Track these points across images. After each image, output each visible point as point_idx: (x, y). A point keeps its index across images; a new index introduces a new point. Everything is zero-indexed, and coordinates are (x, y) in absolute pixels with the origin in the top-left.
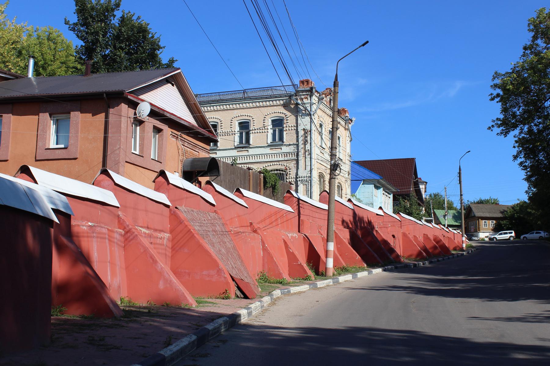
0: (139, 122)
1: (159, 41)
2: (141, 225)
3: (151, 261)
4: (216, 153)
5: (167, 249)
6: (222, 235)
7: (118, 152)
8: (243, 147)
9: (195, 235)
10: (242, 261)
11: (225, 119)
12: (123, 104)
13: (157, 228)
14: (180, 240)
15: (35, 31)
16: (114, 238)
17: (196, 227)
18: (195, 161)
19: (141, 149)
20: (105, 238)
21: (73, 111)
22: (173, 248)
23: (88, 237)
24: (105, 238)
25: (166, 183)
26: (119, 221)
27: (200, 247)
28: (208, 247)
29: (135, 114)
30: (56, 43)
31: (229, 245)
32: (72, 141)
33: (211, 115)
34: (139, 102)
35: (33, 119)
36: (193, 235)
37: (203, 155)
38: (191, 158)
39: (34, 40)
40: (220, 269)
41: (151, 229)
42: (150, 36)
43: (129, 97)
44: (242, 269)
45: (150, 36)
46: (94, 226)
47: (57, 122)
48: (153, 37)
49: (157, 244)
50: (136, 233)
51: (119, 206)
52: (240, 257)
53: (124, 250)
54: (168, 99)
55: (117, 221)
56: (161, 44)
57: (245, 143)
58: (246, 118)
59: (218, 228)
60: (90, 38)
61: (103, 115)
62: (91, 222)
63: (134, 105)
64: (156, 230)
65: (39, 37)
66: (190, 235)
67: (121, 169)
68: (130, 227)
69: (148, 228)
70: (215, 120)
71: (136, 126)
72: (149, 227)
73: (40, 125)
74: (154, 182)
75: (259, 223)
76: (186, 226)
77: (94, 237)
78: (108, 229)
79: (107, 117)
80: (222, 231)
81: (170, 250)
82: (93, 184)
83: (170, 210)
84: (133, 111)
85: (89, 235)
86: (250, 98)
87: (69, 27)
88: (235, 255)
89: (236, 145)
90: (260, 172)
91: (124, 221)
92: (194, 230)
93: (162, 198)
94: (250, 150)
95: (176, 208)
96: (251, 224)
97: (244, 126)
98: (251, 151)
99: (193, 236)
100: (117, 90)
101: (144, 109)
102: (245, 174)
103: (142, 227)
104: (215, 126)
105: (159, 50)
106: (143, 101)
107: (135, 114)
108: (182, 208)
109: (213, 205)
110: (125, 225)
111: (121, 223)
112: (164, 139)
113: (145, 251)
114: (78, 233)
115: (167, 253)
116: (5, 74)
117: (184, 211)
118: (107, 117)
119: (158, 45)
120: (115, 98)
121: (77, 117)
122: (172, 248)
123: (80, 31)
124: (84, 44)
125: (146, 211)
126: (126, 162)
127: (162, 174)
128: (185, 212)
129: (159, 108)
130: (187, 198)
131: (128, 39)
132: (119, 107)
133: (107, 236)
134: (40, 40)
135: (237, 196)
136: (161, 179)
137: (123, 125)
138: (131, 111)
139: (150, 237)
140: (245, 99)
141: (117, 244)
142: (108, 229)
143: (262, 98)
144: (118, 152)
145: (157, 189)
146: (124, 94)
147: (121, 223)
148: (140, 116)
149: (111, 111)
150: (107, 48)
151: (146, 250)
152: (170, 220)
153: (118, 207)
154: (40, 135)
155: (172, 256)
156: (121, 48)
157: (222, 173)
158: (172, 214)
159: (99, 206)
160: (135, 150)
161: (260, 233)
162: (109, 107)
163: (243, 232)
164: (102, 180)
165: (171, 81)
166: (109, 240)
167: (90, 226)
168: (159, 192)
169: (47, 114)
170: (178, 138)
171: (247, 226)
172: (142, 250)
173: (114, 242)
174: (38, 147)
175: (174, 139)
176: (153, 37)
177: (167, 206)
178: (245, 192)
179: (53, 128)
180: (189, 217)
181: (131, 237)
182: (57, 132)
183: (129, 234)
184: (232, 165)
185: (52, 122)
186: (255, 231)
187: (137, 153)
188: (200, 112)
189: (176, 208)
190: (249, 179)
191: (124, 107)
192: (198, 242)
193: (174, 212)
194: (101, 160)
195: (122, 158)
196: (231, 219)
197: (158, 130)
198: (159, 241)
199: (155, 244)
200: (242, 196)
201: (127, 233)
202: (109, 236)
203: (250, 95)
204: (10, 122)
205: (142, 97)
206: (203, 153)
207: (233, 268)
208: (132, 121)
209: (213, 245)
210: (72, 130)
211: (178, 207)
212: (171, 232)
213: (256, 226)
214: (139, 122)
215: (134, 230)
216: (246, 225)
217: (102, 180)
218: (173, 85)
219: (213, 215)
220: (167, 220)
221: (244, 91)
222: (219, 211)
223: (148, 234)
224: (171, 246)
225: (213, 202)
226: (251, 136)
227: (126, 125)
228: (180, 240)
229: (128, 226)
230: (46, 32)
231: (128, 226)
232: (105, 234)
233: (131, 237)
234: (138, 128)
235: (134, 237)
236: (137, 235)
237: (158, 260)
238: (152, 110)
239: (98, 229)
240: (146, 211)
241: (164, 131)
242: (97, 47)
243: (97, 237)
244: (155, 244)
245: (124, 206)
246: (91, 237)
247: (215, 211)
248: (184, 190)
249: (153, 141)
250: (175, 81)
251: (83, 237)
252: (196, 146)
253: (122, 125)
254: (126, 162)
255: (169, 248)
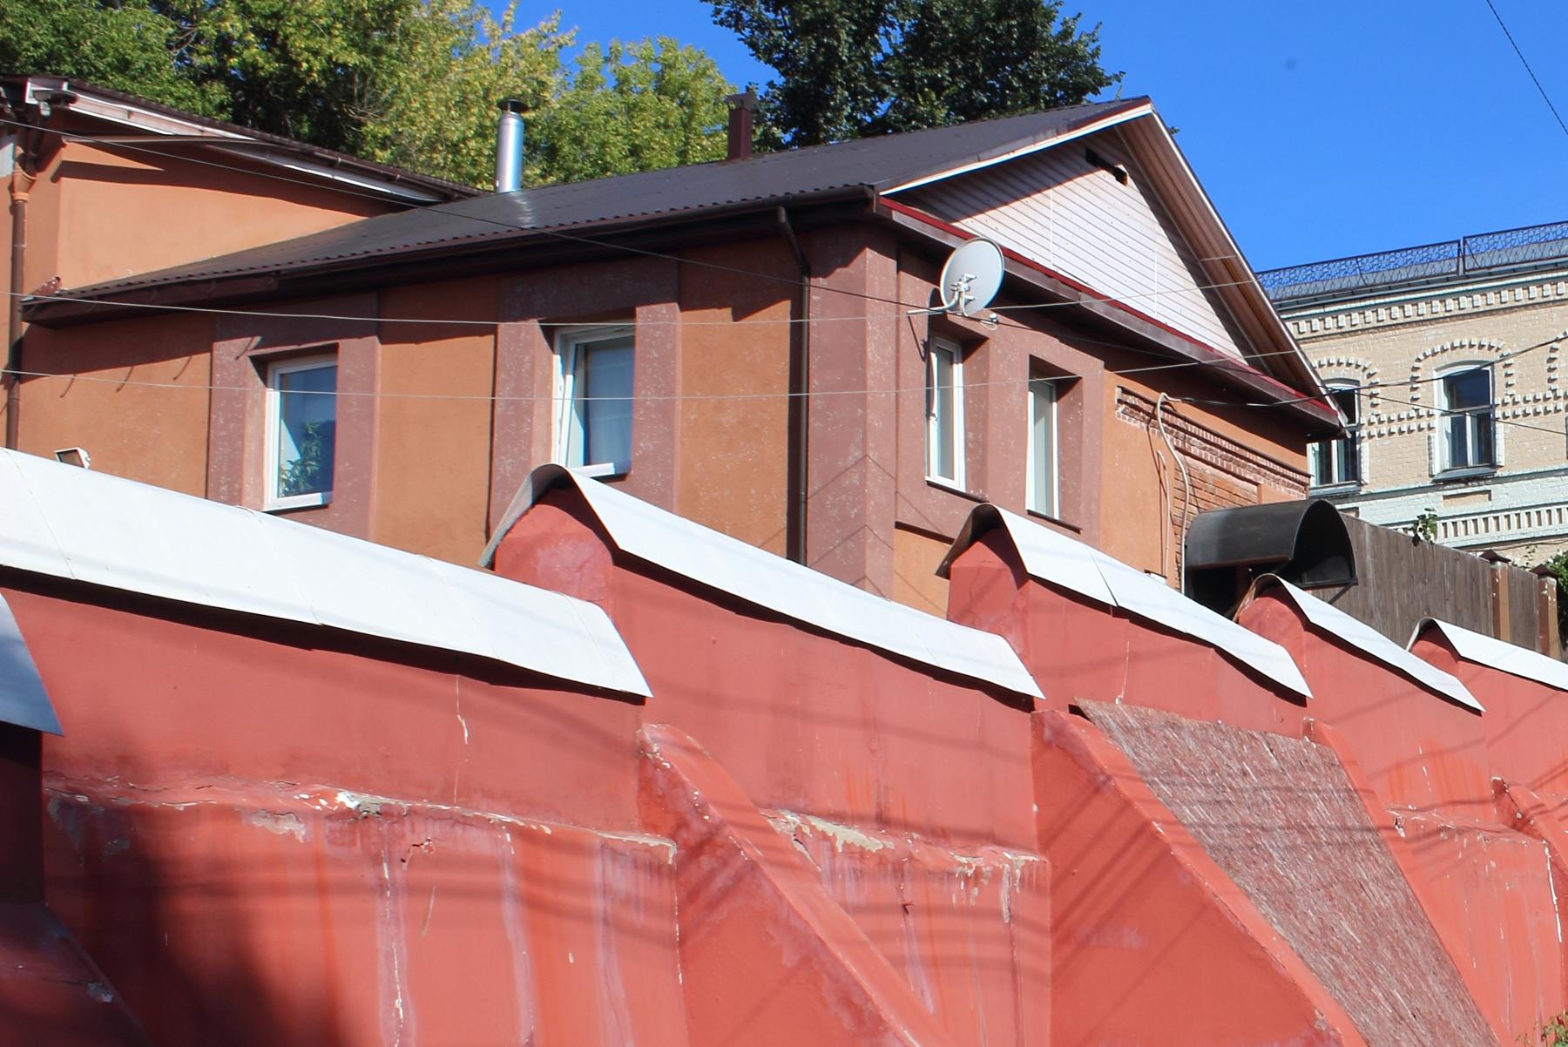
0: (954, 339)
1: (1095, 55)
2: (830, 805)
3: (847, 1021)
4: (1356, 509)
5: (1023, 934)
6: (1342, 846)
7: (855, 479)
8: (1466, 480)
9: (1177, 851)
10: (1455, 976)
11: (1378, 360)
12: (870, 254)
13: (947, 819)
14: (1094, 883)
15: (607, 60)
16: (584, 889)
17: (1184, 811)
18: (1240, 521)
19: (977, 469)
20: (495, 894)
21: (643, 304)
22: (1061, 930)
23: (322, 889)
24: (495, 894)
25: (1009, 577)
26: (646, 785)
27: (1206, 911)
28: (1256, 916)
29: (936, 299)
30: (691, 104)
31: (1378, 896)
32: (644, 445)
33: (1329, 351)
34: (950, 241)
35: (469, 351)
36: (1166, 850)
37: (1278, 492)
38: (1220, 507)
39: (602, 98)
40: (1319, 1035)
41: (907, 826)
42: (1055, 28)
43: (897, 217)
44: (1456, 1017)
45: (1055, 28)
46: (385, 813)
47: (583, 359)
48: (1066, 34)
49: (947, 910)
50: (751, 852)
51: (642, 689)
52: (1442, 955)
53: (684, 961)
54: (1096, 236)
55: (634, 783)
56: (1105, 65)
57: (1475, 459)
58: (1476, 355)
59: (1319, 812)
60: (803, 49)
61: (786, 306)
62: (354, 785)
63: (926, 259)
64: (938, 834)
65: (622, 85)
66: (1146, 853)
67: (874, 562)
68: (714, 814)
69: (883, 821)
70: (1344, 372)
71: (948, 359)
72: (895, 813)
73: (501, 376)
74: (945, 572)
75: (1537, 786)
76: (1127, 804)
77: (382, 887)
78: (525, 836)
79: (799, 311)
80: (1345, 829)
81: (1048, 943)
82: (491, 566)
83: (1038, 724)
84: (926, 288)
85: (332, 875)
86: (1490, 273)
87: (718, 12)
88: (1415, 948)
89: (1437, 470)
90: (1542, 571)
91: (674, 781)
92: (1174, 823)
93: (991, 656)
94: (1496, 488)
95: (1075, 710)
96: (1500, 789)
97: (1470, 390)
98: (1503, 495)
99: (1163, 859)
100: (838, 185)
101: (974, 275)
102: (1474, 580)
103: (838, 817)
104: (1346, 401)
105: (1096, 92)
106: (966, 237)
107: (936, 299)
108: (1111, 711)
109: (1297, 699)
110: (683, 805)
111: (659, 800)
112: (1088, 420)
113: (805, 961)
114: (221, 865)
115: (1024, 958)
116: (389, 179)
117: (1118, 730)
118: (799, 311)
119: (1092, 71)
120: (835, 226)
121: (660, 323)
122: (1057, 924)
123: (762, 26)
124: (780, 80)
125: (870, 724)
126: (899, 526)
127: (987, 527)
128: (1128, 730)
129: (1050, 274)
130: (1135, 657)
131: (963, 46)
132: (851, 269)
133: (509, 880)
134: (633, 98)
135: (1428, 658)
136: (981, 555)
137: (877, 352)
138: (915, 289)
139: (898, 871)
140: (1467, 278)
141: (612, 923)
142: (525, 836)
143: (1537, 270)
144: (855, 479)
145: (962, 613)
146: (869, 201)
147: (659, 800)
148: (955, 307)
149: (819, 291)
150: (883, 95)
151: (812, 956)
152: (1037, 776)
153: (637, 700)
154: (504, 420)
155: (1056, 975)
156: (936, 85)
157: (1371, 575)
158: (1048, 745)
159: (456, 686)
160: (947, 468)
161: (1547, 833)
162: (809, 272)
163: (1461, 832)
164: (543, 540)
165: (1105, 156)
166: (532, 904)
167: (345, 814)
168: (973, 625)
169: (534, 326)
170: (1153, 416)
171: (1482, 802)
172: (789, 959)
173: (585, 917)
174: (496, 478)
175: (1136, 424)
176: (1066, 34)
177: (1021, 702)
178: (1465, 640)
179: (563, 387)
180: (1150, 756)
181: (721, 881)
182: (587, 415)
183: (706, 862)
184: (1416, 540)
185: (557, 359)
186: (1521, 825)
187: (959, 484)
188: (1276, 339)
189: (1075, 710)
190: (1496, 601)
191: (875, 266)
192: (1196, 886)
193: (1059, 732)
194: (782, 521)
195: (878, 505)
196: (1399, 766)
197: (1054, 384)
198: (956, 894)
199: (929, 911)
200: (1452, 658)
201: (693, 852)
202: (529, 874)
203: (1485, 260)
204: (372, 376)
205: (966, 224)
206: (1280, 481)
207: (1398, 1018)
208: (923, 334)
209: (1285, 900)
210: (645, 396)
211: (1082, 703)
212: (1046, 841)
213: (1524, 797)
214: (954, 339)
215: (733, 835)
216: (1473, 795)
217: (543, 540)
218: (1121, 177)
219: (1287, 745)
220: (1024, 778)
221: (1462, 246)
222: (1326, 728)
223: (881, 858)
224: (1047, 922)
225: (1298, 684)
226: (1501, 430)
227: (890, 350)
228: (1094, 883)
229: (700, 810)
230: (647, 59)
231: (700, 810)
232: (494, 865)
233: (721, 881)
234: (958, 369)
235: (738, 879)
236: (753, 866)
237: (889, 1015)
238: (1008, 281)
239: (427, 834)
240: (870, 724)
241: (1086, 384)
242: (834, 85)
243: (415, 890)
244: (929, 911)
245: (684, 693)
246: (353, 889)
247: (1307, 730)
248: (1120, 612)
249: (1036, 435)
250: (1124, 152)
251: (279, 890)
252: (1241, 453)
253: (872, 352)
254: (899, 526)
255: (1035, 928)
